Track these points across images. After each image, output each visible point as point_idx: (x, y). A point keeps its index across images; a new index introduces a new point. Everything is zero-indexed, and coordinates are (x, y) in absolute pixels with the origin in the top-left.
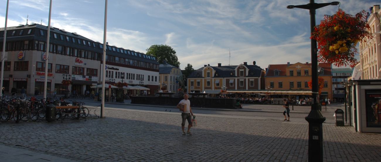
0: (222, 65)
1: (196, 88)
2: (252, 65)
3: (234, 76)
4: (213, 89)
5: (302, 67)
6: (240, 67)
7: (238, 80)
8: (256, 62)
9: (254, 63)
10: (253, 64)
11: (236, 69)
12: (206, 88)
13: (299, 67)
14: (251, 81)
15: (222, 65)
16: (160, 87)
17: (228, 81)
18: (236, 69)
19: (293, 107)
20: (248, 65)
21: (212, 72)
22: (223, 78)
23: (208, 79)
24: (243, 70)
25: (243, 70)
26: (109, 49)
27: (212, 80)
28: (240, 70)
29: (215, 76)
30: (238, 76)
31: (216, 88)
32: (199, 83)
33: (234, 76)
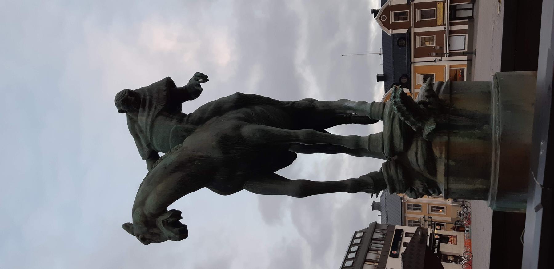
0: (382, 73)
3: (405, 39)
11: (390, 32)
15: (382, 73)
18: (390, 32)
19: (466, 60)
24: (392, 14)
25: (392, 14)
26: (354, 257)
28: (392, 20)
33: (405, 39)
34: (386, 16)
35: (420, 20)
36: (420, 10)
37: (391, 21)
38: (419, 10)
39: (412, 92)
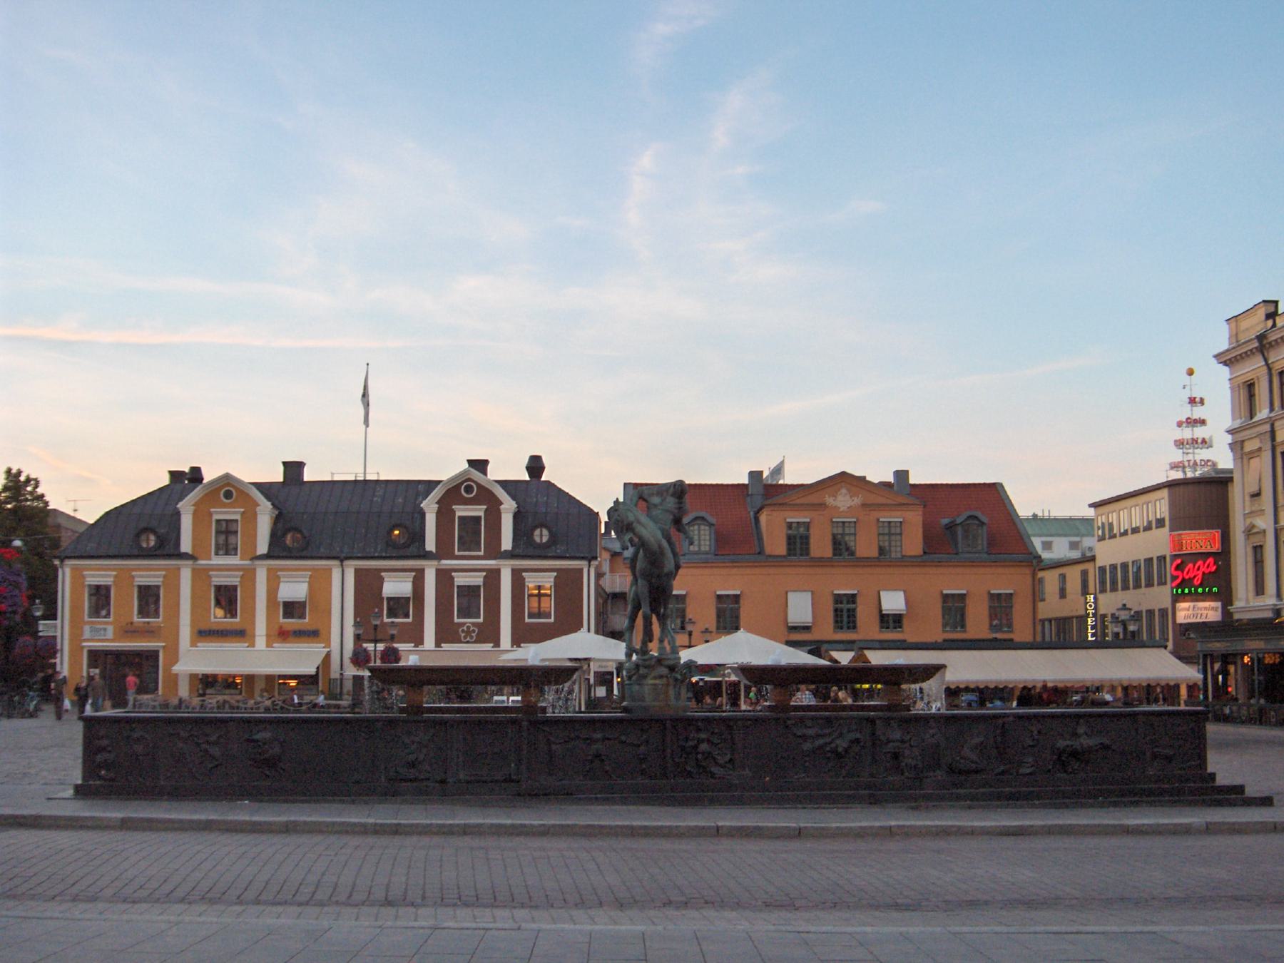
1: (129, 631)
2: (541, 477)
3: (411, 546)
4: (261, 642)
5: (864, 505)
6: (457, 491)
7: (444, 577)
8: (545, 460)
9: (535, 466)
10: (526, 477)
11: (430, 506)
12: (204, 633)
13: (843, 501)
14: (458, 587)
15: (308, 476)
16: (1276, 605)
17: (368, 588)
18: (430, 506)
20: (90, 514)
21: (250, 517)
22: (337, 563)
23: (225, 568)
24: (478, 511)
25: (478, 511)
27: (249, 575)
28: (461, 511)
29: (278, 549)
30: (444, 550)
31: (283, 635)
32: (149, 598)
33: (411, 546)
34: (219, 498)
35: (456, 584)
36: (482, 584)
37: (460, 510)
38: (482, 579)
39: (257, 562)
